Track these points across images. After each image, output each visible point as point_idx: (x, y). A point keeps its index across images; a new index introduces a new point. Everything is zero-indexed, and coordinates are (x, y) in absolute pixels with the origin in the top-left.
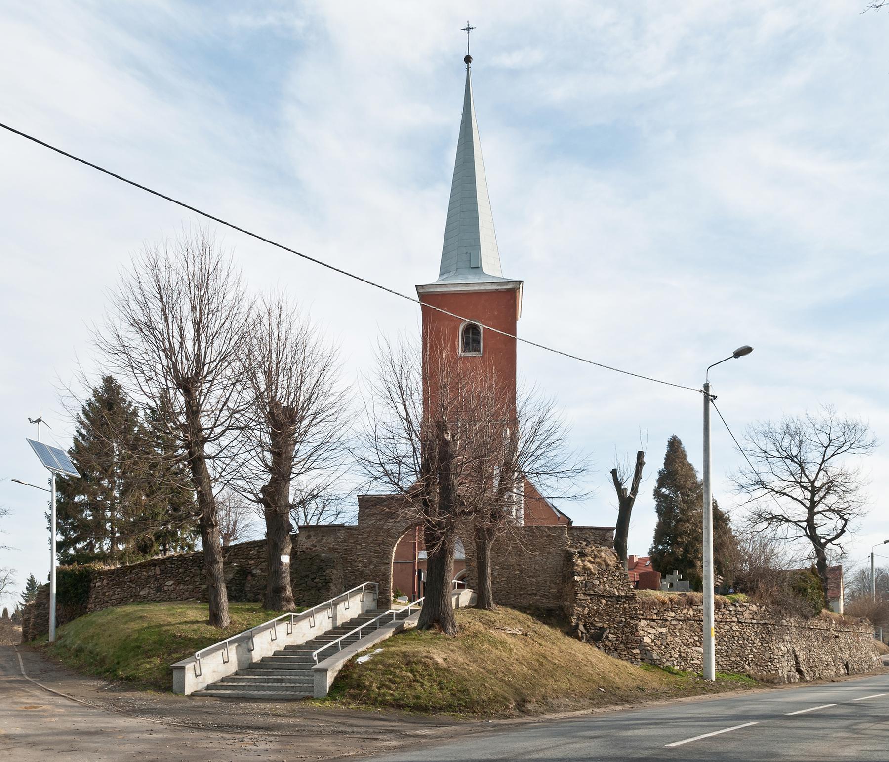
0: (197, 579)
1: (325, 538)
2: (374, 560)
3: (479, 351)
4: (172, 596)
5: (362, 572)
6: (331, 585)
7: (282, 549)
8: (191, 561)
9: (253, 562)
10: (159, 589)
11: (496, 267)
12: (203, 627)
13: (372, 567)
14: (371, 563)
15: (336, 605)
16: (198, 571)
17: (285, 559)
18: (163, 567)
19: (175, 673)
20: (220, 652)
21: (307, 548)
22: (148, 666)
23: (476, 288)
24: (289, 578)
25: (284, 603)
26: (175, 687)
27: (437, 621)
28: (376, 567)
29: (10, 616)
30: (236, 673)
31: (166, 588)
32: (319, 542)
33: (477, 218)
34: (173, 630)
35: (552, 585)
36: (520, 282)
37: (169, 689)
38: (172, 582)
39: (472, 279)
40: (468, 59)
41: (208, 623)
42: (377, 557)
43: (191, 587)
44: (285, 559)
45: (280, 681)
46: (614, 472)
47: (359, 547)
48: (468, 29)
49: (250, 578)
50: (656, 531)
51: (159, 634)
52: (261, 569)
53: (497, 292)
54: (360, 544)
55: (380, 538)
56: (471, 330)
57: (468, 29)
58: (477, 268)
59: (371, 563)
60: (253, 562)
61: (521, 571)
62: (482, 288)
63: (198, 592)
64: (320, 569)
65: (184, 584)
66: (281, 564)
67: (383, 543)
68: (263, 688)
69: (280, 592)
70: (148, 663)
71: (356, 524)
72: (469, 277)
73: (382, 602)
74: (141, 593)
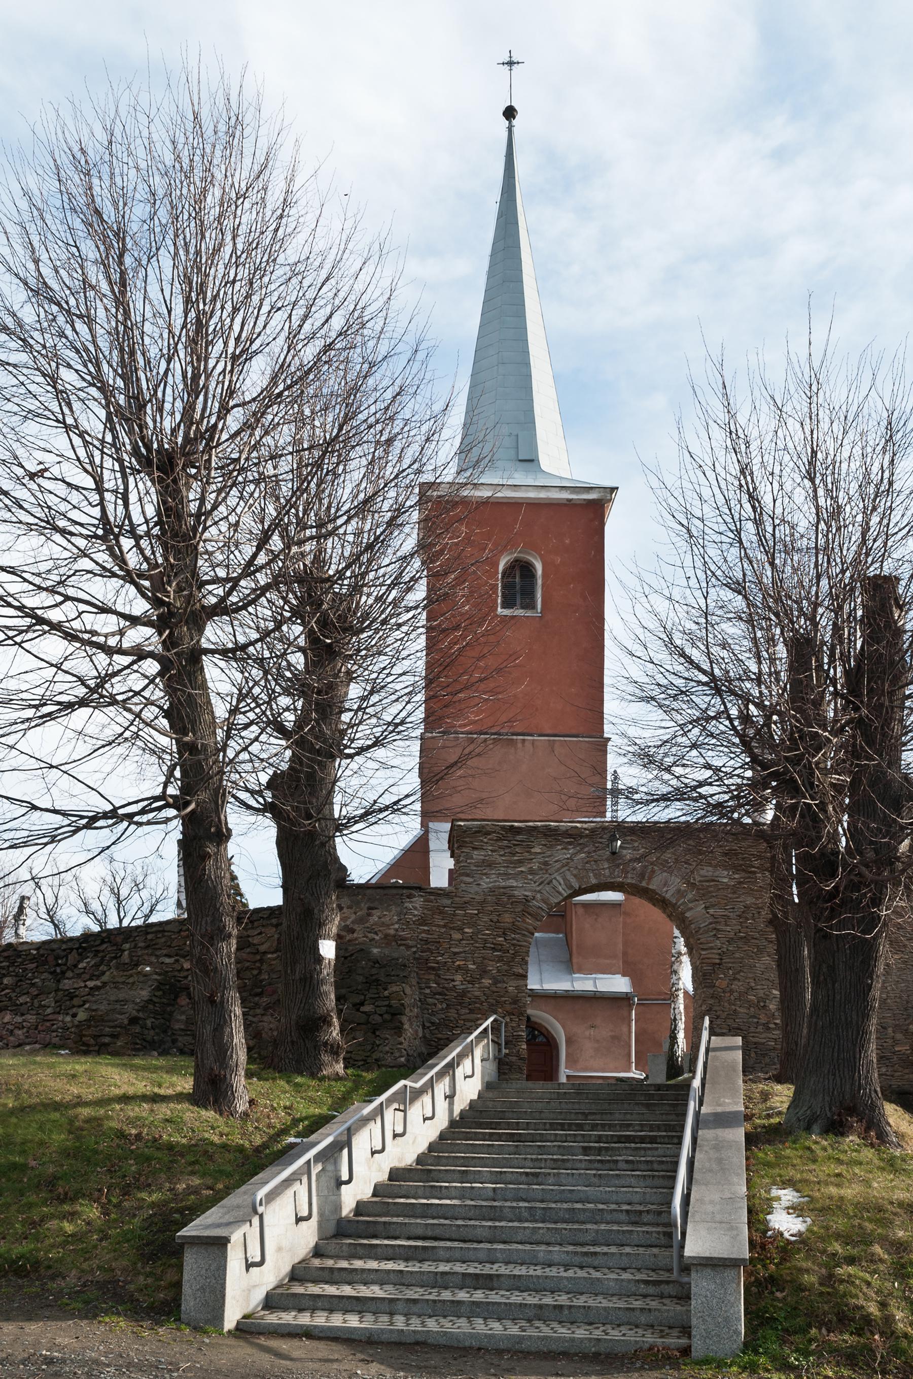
0: (49, 1001)
1: (376, 913)
2: (492, 967)
3: (532, 606)
5: (464, 993)
6: (404, 1019)
7: (321, 925)
8: (34, 959)
11: (563, 460)
12: (190, 1114)
13: (487, 982)
14: (484, 972)
15: (451, 1067)
16: (52, 984)
17: (328, 949)
19: (192, 1262)
20: (289, 1193)
22: (69, 1227)
23: (532, 494)
24: (333, 996)
25: (326, 1058)
26: (189, 1302)
27: (851, 1110)
28: (496, 982)
29: (653, 736)
30: (317, 1252)
32: (361, 920)
33: (529, 376)
34: (117, 1117)
35: (899, 1036)
36: (613, 489)
37: (165, 1308)
39: (520, 478)
40: (510, 113)
41: (197, 1098)
43: (31, 1018)
44: (328, 949)
45: (487, 1282)
47: (457, 936)
48: (511, 63)
49: (183, 1001)
51: (73, 1129)
53: (569, 504)
54: (460, 930)
55: (507, 918)
56: (522, 569)
57: (511, 63)
58: (531, 461)
59: (484, 972)
62: (543, 495)
63: (49, 1030)
64: (372, 982)
65: (15, 1013)
66: (319, 959)
67: (515, 929)
68: (455, 1309)
69: (318, 1028)
70: (64, 1217)
73: (510, 1065)
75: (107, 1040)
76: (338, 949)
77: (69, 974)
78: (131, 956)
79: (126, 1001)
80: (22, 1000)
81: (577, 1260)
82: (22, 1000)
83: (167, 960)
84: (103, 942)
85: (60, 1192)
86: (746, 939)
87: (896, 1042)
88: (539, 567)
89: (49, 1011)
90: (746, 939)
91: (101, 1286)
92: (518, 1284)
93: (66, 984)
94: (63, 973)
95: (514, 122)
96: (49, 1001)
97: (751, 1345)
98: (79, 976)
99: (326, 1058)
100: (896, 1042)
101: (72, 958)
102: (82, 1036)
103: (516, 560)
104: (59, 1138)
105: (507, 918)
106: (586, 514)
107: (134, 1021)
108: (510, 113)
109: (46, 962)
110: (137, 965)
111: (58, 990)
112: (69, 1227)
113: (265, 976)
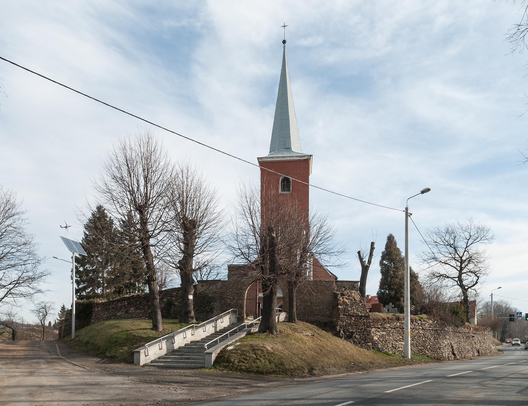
0: (146, 307)
2: (236, 298)
3: (289, 190)
5: (230, 304)
7: (189, 292)
8: (143, 298)
12: (149, 331)
13: (235, 301)
14: (234, 299)
15: (216, 320)
17: (191, 297)
18: (129, 301)
23: (288, 159)
25: (190, 319)
26: (135, 362)
27: (268, 329)
30: (166, 355)
32: (208, 288)
34: (134, 333)
36: (311, 156)
37: (131, 362)
38: (133, 309)
39: (286, 154)
40: (284, 42)
41: (152, 329)
42: (237, 296)
43: (143, 311)
44: (191, 297)
45: (188, 359)
48: (284, 26)
49: (173, 307)
57: (284, 26)
58: (289, 149)
59: (234, 299)
61: (311, 303)
62: (291, 159)
66: (189, 299)
69: (188, 314)
71: (227, 279)
76: (193, 297)
85: (122, 345)
87: (326, 312)
91: (123, 359)
92: (193, 359)
96: (146, 307)
99: (190, 319)
100: (326, 312)
104: (125, 336)
112: (121, 351)
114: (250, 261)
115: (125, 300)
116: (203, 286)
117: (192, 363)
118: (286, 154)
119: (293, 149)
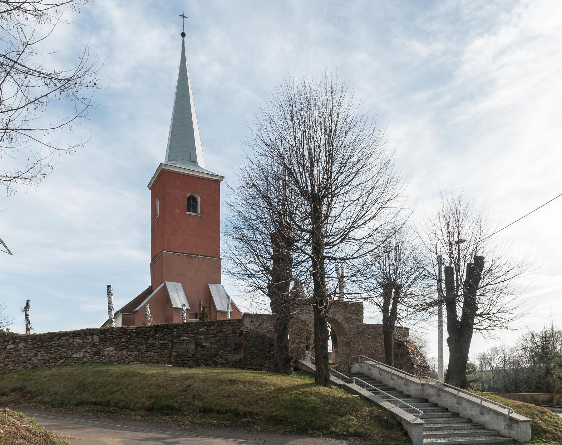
0: (144, 347)
3: (196, 211)
4: (113, 359)
9: (203, 337)
10: (97, 353)
13: (295, 344)
18: (102, 336)
21: (251, 329)
23: (198, 174)
28: (298, 344)
31: (105, 353)
36: (223, 177)
38: (112, 349)
39: (192, 168)
40: (183, 35)
42: (299, 338)
46: (28, 301)
50: (48, 333)
52: (211, 343)
58: (195, 162)
60: (203, 337)
61: (375, 351)
62: (201, 175)
71: (270, 312)
72: (191, 166)
74: (74, 356)
75: (186, 362)
77: (151, 338)
78: (177, 333)
79: (188, 349)
80: (131, 346)
81: (446, 422)
82: (131, 346)
83: (192, 335)
84: (165, 328)
86: (357, 334)
88: (199, 200)
89: (143, 351)
90: (357, 334)
93: (150, 342)
94: (148, 338)
95: (185, 38)
96: (144, 347)
97: (533, 438)
98: (156, 339)
101: (152, 333)
102: (176, 360)
103: (191, 196)
105: (300, 326)
106: (212, 184)
107: (193, 355)
108: (183, 35)
109: (140, 334)
110: (180, 336)
111: (147, 344)
113: (228, 341)
114: (342, 294)
115: (93, 334)
116: (252, 321)
117: (446, 436)
118: (192, 168)
119: (201, 163)
